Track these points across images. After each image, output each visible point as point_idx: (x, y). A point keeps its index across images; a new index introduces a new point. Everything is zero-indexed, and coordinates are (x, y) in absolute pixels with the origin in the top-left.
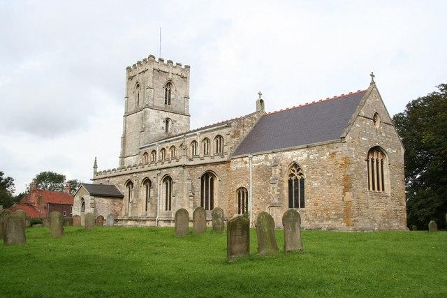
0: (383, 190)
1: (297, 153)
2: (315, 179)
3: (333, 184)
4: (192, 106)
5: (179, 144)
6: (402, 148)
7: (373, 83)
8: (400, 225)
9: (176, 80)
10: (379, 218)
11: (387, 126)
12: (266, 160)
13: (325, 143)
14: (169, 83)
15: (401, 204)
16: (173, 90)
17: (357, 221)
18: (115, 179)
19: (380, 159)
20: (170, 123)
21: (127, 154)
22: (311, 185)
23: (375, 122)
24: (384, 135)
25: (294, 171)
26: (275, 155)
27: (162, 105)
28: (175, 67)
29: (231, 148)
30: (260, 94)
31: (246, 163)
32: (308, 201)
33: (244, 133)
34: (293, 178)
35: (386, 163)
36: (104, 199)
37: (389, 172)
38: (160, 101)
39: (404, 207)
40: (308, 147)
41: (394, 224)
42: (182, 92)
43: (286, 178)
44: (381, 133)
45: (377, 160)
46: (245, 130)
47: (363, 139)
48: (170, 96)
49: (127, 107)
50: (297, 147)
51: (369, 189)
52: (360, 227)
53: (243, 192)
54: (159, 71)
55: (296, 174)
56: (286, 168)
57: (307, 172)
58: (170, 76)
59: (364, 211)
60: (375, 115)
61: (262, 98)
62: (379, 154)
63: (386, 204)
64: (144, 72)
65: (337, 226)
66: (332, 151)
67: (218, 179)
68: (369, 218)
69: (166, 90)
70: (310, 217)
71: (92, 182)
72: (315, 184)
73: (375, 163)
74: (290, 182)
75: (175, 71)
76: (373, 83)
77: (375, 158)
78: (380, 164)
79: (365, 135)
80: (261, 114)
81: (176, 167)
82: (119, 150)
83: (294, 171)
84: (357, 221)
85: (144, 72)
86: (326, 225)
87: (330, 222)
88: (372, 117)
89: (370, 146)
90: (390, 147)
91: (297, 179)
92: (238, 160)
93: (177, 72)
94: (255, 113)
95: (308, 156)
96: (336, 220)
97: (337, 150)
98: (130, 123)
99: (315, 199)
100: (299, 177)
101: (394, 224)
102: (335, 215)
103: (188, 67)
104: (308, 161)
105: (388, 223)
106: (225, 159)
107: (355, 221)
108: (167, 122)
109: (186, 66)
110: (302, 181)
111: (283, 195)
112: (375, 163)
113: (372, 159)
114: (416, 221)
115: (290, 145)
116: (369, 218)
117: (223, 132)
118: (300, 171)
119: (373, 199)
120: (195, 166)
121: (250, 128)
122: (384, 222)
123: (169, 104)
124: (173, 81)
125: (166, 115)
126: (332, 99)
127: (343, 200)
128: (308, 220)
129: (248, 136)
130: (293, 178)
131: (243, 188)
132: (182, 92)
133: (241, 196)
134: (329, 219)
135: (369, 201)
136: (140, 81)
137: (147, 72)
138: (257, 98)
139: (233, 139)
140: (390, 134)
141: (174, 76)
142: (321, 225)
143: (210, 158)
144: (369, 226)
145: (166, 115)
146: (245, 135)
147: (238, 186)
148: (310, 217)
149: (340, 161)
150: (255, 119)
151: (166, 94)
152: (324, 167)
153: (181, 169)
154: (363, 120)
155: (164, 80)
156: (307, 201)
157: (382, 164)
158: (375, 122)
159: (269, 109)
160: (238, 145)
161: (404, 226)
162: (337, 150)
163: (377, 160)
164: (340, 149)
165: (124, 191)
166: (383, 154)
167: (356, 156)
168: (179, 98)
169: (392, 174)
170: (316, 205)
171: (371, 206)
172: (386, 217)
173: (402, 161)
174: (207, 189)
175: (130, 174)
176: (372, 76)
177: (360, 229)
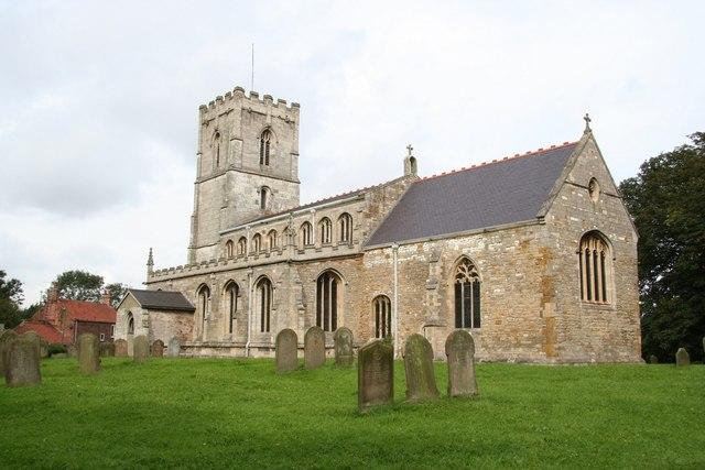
0: (604, 299)
1: (468, 241)
2: (497, 283)
3: (524, 291)
4: (303, 168)
5: (283, 228)
6: (634, 233)
7: (588, 131)
8: (630, 354)
9: (277, 125)
10: (597, 344)
11: (611, 199)
12: (420, 252)
13: (512, 225)
14: (267, 132)
15: (633, 322)
16: (273, 142)
17: (564, 349)
18: (181, 282)
19: (599, 251)
20: (268, 194)
21: (201, 243)
22: (491, 291)
23: (591, 192)
24: (605, 212)
25: (463, 269)
26: (433, 244)
27: (256, 165)
28: (276, 106)
29: (365, 234)
30: (410, 149)
31: (388, 257)
32: (486, 317)
33: (385, 210)
34: (462, 281)
35: (609, 257)
36: (164, 314)
37: (613, 271)
38: (253, 160)
39: (637, 326)
40: (485, 232)
41: (621, 354)
42: (287, 146)
43: (451, 281)
44: (600, 210)
45: (595, 252)
46: (387, 205)
47: (572, 218)
48: (268, 152)
49: (200, 169)
50: (468, 232)
51: (582, 298)
52: (568, 358)
53: (384, 303)
54: (251, 112)
55: (467, 274)
56: (451, 265)
57: (484, 272)
58: (268, 120)
59: (574, 332)
60: (591, 182)
61: (414, 154)
62: (598, 243)
63: (609, 322)
64: (227, 113)
65: (532, 357)
66: (523, 238)
67: (344, 283)
68: (582, 345)
69: (262, 141)
70: (489, 342)
71: (145, 288)
72: (498, 291)
73: (591, 258)
74: (457, 286)
75: (276, 112)
76: (588, 131)
77: (592, 249)
78: (599, 259)
79: (575, 213)
80: (412, 180)
81: (278, 263)
82: (187, 237)
83: (463, 269)
84: (564, 349)
85: (227, 113)
86: (513, 354)
87: (520, 350)
88: (586, 184)
89: (584, 231)
90: (615, 232)
91: (468, 283)
92: (376, 252)
93: (279, 113)
94: (403, 178)
95: (487, 246)
96: (530, 346)
97: (531, 236)
98: (205, 194)
99: (496, 314)
100: (472, 280)
101: (621, 354)
102: (528, 339)
103: (296, 106)
104: (486, 253)
105: (611, 351)
106: (355, 250)
107: (559, 348)
108: (264, 192)
109: (293, 105)
110: (477, 285)
111: (447, 308)
112: (591, 258)
113: (587, 251)
114: (656, 349)
115: (457, 228)
116: (582, 345)
117: (352, 209)
118: (473, 270)
119: (589, 314)
120: (308, 261)
121: (395, 203)
122: (605, 351)
123: (267, 164)
124: (273, 127)
125: (262, 181)
126: (524, 157)
127: (541, 316)
128: (486, 347)
129: (391, 214)
130: (462, 281)
131: (383, 296)
132: (287, 146)
133: (381, 309)
134: (518, 345)
135: (582, 317)
136: (221, 128)
137: (232, 113)
138: (406, 154)
139: (368, 220)
140: (616, 211)
141: (275, 120)
142: (506, 354)
143: (331, 249)
144: (581, 356)
145: (262, 181)
146: (387, 212)
147: (376, 294)
148: (489, 342)
149: (537, 255)
150: (403, 187)
151: (262, 148)
152: (511, 264)
153: (286, 266)
154: (573, 190)
155: (259, 126)
156: (484, 317)
157: (603, 258)
158: (591, 192)
159: (424, 172)
160: (376, 228)
161: (637, 357)
162: (531, 236)
163: (595, 252)
164: (536, 236)
165: (195, 301)
166: (604, 243)
167: (562, 247)
168: (282, 155)
169: (618, 274)
170: (499, 323)
171: (585, 325)
172: (609, 342)
173: (634, 254)
174: (326, 298)
175: (205, 274)
176: (587, 120)
177: (568, 361)
